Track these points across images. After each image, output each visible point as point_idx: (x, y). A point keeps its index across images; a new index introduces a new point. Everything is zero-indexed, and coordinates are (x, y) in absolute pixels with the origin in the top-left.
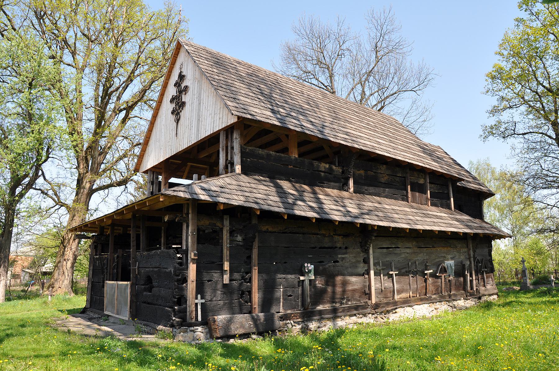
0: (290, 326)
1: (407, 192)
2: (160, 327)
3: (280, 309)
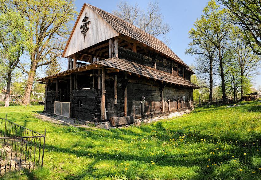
0: (137, 121)
1: (172, 70)
2: (87, 122)
3: (134, 115)
